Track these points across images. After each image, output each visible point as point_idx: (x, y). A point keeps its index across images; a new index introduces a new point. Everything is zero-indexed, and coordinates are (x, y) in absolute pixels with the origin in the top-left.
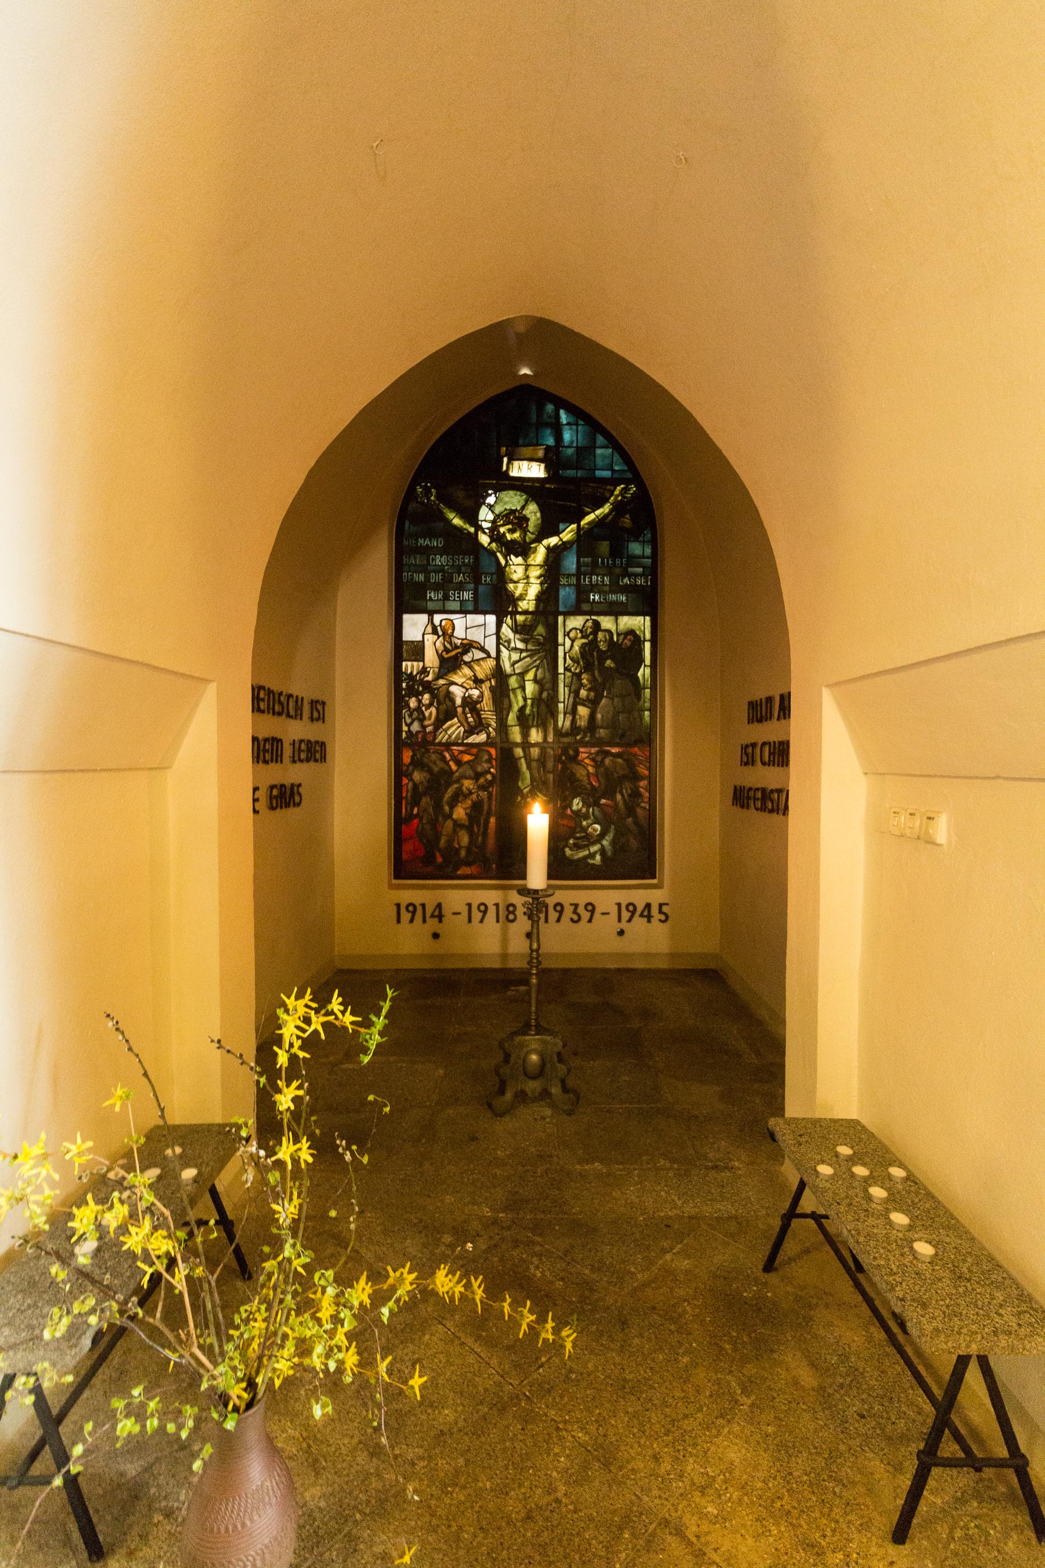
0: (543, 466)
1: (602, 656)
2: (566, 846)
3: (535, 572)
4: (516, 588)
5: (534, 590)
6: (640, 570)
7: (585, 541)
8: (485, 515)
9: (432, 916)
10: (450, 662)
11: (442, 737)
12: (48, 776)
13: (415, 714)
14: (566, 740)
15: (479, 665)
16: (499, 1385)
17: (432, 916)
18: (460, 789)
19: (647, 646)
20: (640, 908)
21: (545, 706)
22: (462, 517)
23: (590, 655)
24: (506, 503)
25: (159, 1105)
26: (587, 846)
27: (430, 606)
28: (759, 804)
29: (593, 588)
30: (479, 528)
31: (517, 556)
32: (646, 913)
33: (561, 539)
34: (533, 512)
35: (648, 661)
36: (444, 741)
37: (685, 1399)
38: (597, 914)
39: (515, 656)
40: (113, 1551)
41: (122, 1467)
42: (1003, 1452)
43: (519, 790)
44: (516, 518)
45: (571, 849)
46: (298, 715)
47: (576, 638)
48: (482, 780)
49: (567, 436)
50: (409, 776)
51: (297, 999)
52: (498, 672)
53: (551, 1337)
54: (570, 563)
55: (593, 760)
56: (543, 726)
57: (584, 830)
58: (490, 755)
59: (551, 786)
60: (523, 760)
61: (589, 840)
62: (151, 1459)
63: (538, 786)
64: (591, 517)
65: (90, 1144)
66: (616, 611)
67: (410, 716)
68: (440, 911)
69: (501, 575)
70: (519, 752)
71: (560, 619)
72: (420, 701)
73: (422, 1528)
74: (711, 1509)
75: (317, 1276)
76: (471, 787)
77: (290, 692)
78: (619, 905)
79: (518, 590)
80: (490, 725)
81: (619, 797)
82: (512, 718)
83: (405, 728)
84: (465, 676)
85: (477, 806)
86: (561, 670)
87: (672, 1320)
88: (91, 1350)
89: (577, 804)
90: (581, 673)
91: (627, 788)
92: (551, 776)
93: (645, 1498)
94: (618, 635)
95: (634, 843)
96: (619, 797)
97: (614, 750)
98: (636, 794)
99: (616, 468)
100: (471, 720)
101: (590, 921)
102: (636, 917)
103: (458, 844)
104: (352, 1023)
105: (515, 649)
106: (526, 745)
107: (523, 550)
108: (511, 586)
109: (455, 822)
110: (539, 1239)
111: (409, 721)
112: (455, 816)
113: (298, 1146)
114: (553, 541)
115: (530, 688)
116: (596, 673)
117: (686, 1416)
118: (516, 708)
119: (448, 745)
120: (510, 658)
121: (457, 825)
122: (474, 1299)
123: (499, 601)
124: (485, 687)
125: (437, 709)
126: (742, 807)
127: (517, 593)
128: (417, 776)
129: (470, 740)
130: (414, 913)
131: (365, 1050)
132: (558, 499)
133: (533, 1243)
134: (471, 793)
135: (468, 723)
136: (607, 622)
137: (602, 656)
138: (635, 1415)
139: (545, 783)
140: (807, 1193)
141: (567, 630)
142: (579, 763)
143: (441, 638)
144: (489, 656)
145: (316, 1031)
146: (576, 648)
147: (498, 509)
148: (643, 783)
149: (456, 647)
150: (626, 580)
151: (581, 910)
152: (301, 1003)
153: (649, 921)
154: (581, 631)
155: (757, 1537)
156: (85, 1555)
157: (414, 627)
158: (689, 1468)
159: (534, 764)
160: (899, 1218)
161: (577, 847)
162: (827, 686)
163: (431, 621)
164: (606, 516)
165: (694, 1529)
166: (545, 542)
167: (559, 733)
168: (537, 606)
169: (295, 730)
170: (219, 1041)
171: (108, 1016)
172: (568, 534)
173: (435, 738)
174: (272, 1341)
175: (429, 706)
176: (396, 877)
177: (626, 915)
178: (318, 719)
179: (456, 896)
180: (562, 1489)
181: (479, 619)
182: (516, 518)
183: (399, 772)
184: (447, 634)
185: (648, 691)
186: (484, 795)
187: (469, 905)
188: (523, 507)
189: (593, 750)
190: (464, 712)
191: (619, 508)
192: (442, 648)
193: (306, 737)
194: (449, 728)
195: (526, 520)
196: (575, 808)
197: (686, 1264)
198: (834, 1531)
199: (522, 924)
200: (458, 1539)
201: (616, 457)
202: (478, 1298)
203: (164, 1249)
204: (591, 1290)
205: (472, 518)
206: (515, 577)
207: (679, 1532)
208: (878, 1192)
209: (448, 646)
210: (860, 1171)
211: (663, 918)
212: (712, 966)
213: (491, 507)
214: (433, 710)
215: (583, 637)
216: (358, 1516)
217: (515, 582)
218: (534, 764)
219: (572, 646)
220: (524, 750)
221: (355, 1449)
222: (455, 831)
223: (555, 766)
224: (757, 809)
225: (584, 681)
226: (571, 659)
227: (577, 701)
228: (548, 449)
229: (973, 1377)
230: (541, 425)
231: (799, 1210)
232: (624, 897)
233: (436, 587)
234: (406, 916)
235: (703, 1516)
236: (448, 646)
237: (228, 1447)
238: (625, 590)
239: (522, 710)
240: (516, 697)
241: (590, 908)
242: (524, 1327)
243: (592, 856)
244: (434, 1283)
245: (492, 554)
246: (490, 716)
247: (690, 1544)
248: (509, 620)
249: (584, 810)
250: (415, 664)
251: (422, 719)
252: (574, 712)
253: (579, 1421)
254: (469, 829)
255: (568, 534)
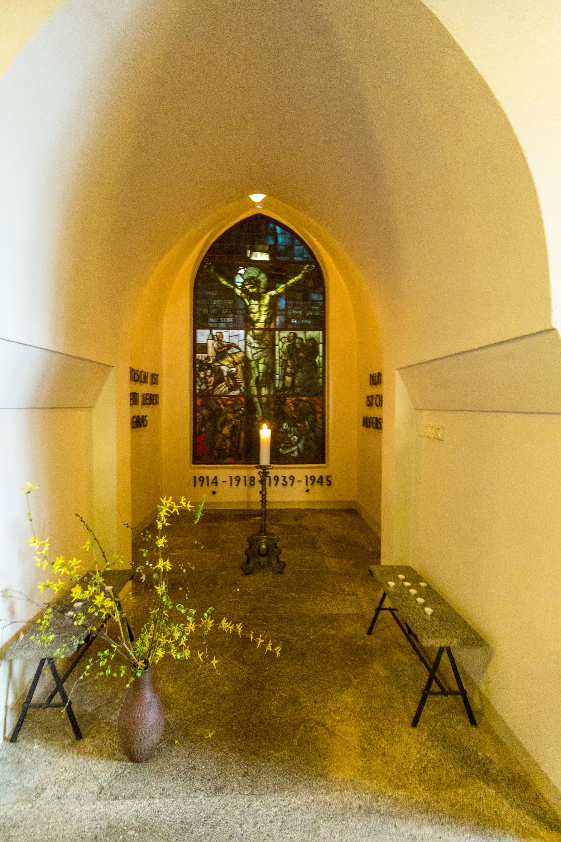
0: (268, 255)
1: (298, 351)
2: (280, 447)
3: (264, 309)
4: (254, 316)
5: (263, 318)
6: (316, 307)
7: (289, 293)
8: (239, 280)
9: (212, 483)
10: (221, 354)
11: (217, 392)
12: (48, 410)
13: (203, 380)
14: (280, 394)
15: (236, 356)
16: (248, 677)
17: (212, 483)
18: (226, 419)
19: (321, 346)
20: (317, 479)
21: (269, 375)
22: (227, 281)
23: (292, 351)
24: (250, 273)
25: (102, 551)
26: (290, 447)
27: (211, 325)
28: (374, 425)
29: (293, 317)
30: (236, 286)
31: (255, 300)
32: (320, 481)
33: (277, 292)
34: (263, 278)
35: (321, 354)
36: (218, 394)
37: (329, 681)
38: (296, 482)
39: (254, 351)
40: (86, 737)
41: (85, 709)
42: (454, 686)
43: (256, 419)
44: (254, 281)
45: (282, 449)
46: (145, 381)
47: (285, 342)
48: (237, 414)
49: (280, 240)
50: (200, 411)
51: (166, 500)
52: (246, 360)
53: (270, 650)
54: (282, 304)
55: (294, 404)
56: (268, 386)
57: (289, 439)
58: (241, 401)
59: (273, 417)
60: (258, 404)
61: (291, 444)
62: (98, 706)
63: (265, 418)
64: (292, 281)
65: (80, 561)
66: (305, 328)
67: (201, 381)
68: (216, 480)
69: (247, 310)
70: (256, 399)
71: (277, 332)
72: (205, 374)
73: (216, 726)
74: (338, 718)
75: (177, 606)
76: (232, 417)
77: (142, 370)
78: (306, 476)
79: (255, 317)
80: (241, 386)
81: (307, 423)
82: (252, 382)
83: (198, 388)
84: (228, 361)
85: (235, 427)
86: (277, 358)
87: (325, 653)
88: (77, 650)
89: (285, 426)
90: (287, 360)
91: (311, 417)
92: (272, 412)
93: (310, 715)
94: (306, 340)
95: (314, 445)
96: (307, 423)
97: (304, 399)
98: (315, 421)
99: (305, 256)
100: (232, 383)
101: (292, 485)
102: (316, 483)
103: (225, 446)
104: (190, 508)
105: (254, 347)
106: (260, 396)
107: (258, 297)
108: (252, 315)
109: (224, 435)
110: (266, 624)
111: (200, 384)
112: (224, 432)
113: (165, 563)
114: (273, 293)
115: (261, 367)
116: (295, 359)
117: (329, 687)
118: (254, 377)
119: (220, 396)
120: (251, 352)
121: (225, 437)
122: (237, 632)
123: (248, 323)
124: (239, 367)
125: (215, 378)
126: (367, 427)
127: (255, 319)
128: (204, 412)
129: (231, 394)
130: (203, 481)
131: (196, 519)
132: (276, 272)
133: (263, 625)
134: (232, 421)
135: (230, 385)
136: (300, 334)
137: (298, 351)
138: (308, 687)
139: (269, 415)
140: (387, 598)
141: (281, 337)
142: (287, 405)
143: (216, 342)
144: (241, 351)
145: (175, 512)
146: (285, 347)
147: (245, 277)
148: (319, 416)
149: (224, 346)
150: (310, 313)
151: (287, 479)
152: (168, 501)
153: (322, 485)
154: (288, 339)
155: (356, 727)
156: (74, 738)
157: (203, 336)
158: (329, 705)
159: (264, 406)
160: (420, 600)
161: (285, 448)
162: (398, 369)
163: (211, 333)
164: (300, 280)
165: (330, 725)
166: (269, 293)
167: (276, 390)
168: (265, 325)
169: (144, 389)
170: (127, 524)
171: (77, 515)
172: (281, 289)
173: (213, 392)
174: (154, 645)
175: (210, 376)
176: (194, 463)
177: (310, 482)
178: (155, 383)
179: (224, 472)
180: (275, 712)
181: (236, 332)
182: (254, 281)
183: (195, 410)
184: (219, 339)
185: (321, 369)
186: (238, 421)
187: (231, 477)
188: (258, 276)
189: (294, 399)
190: (228, 380)
191: (307, 277)
192: (217, 347)
193: (150, 393)
194: (220, 387)
195: (259, 282)
196: (284, 428)
197: (332, 632)
198: (388, 724)
199: (258, 487)
200: (231, 730)
201: (305, 251)
202: (239, 631)
203: (110, 605)
204: (289, 643)
205: (231, 280)
206: (254, 311)
207: (324, 726)
208: (413, 591)
209: (220, 346)
210: (407, 584)
211: (329, 483)
212: (354, 507)
213: (242, 275)
214: (212, 378)
215: (288, 342)
216: (189, 723)
217: (254, 313)
218: (264, 406)
219: (283, 346)
220: (259, 399)
221: (186, 700)
222: (223, 440)
223: (274, 407)
224: (374, 428)
225: (289, 364)
226: (282, 352)
227: (285, 374)
228: (271, 246)
229: (445, 658)
230: (267, 234)
231: (383, 607)
232: (309, 473)
233: (213, 316)
234: (198, 483)
235: (334, 720)
236: (220, 346)
237: (137, 684)
238: (308, 317)
239: (257, 378)
240: (254, 372)
241: (292, 478)
242: (259, 644)
243: (293, 452)
244: (221, 625)
245: (242, 298)
246: (241, 381)
247: (328, 729)
248: (251, 333)
249: (289, 429)
250: (203, 355)
251: (206, 383)
252: (284, 379)
253: (283, 690)
254: (231, 438)
255: (281, 289)
